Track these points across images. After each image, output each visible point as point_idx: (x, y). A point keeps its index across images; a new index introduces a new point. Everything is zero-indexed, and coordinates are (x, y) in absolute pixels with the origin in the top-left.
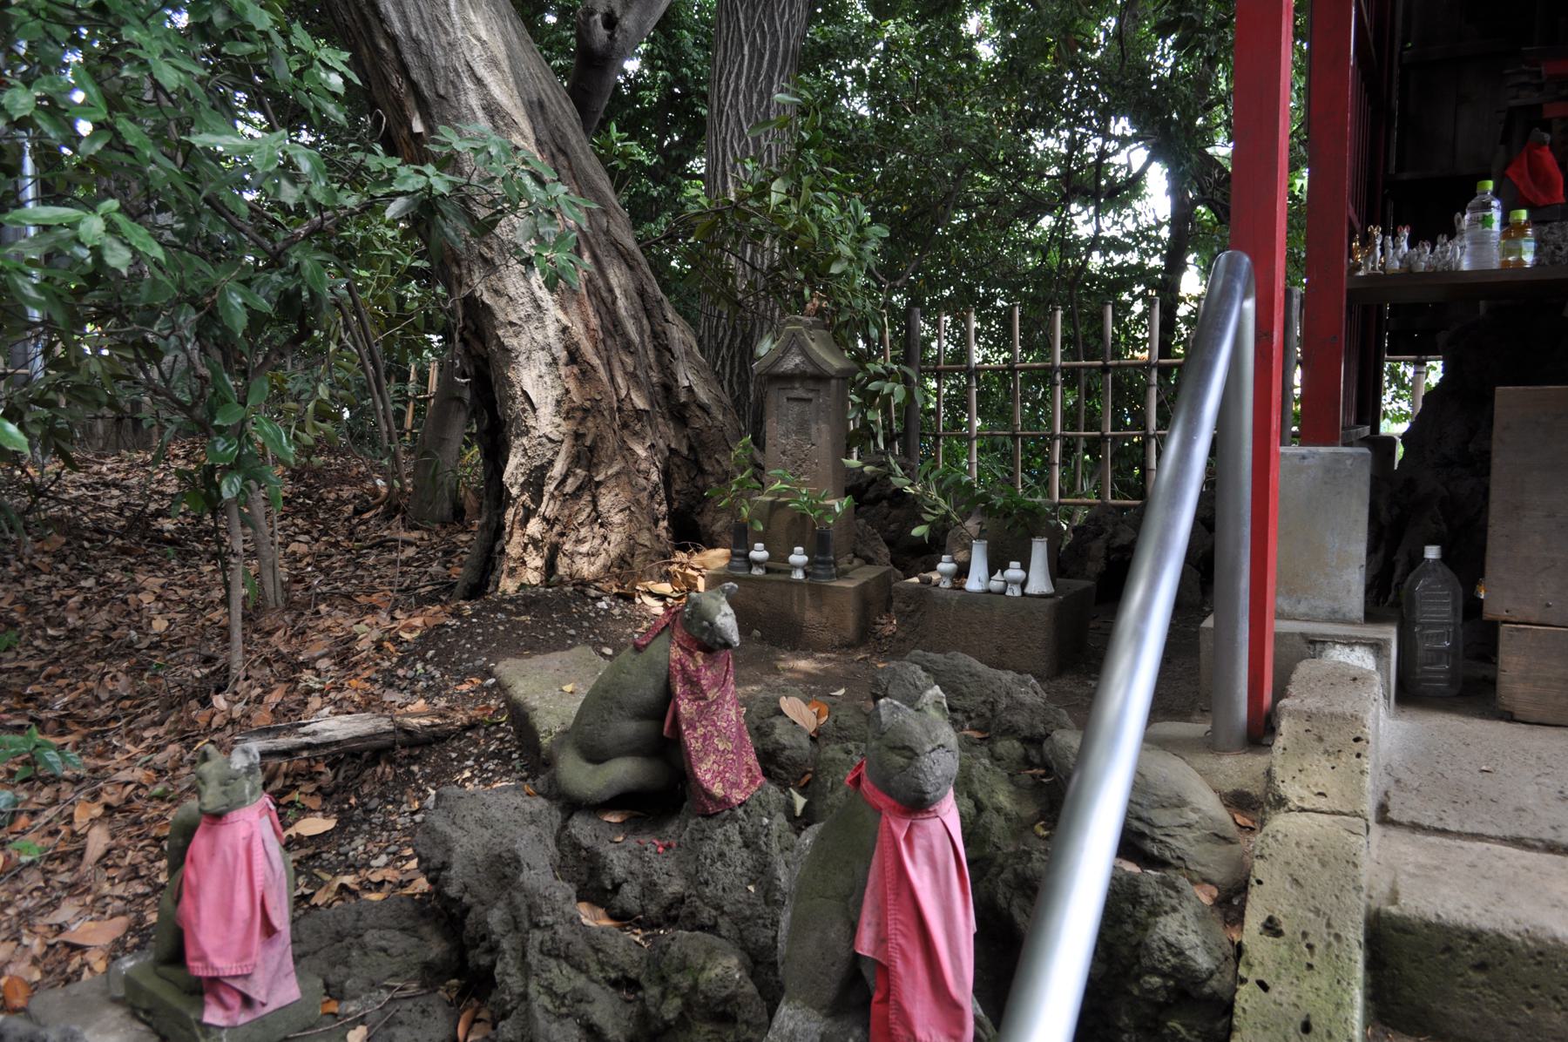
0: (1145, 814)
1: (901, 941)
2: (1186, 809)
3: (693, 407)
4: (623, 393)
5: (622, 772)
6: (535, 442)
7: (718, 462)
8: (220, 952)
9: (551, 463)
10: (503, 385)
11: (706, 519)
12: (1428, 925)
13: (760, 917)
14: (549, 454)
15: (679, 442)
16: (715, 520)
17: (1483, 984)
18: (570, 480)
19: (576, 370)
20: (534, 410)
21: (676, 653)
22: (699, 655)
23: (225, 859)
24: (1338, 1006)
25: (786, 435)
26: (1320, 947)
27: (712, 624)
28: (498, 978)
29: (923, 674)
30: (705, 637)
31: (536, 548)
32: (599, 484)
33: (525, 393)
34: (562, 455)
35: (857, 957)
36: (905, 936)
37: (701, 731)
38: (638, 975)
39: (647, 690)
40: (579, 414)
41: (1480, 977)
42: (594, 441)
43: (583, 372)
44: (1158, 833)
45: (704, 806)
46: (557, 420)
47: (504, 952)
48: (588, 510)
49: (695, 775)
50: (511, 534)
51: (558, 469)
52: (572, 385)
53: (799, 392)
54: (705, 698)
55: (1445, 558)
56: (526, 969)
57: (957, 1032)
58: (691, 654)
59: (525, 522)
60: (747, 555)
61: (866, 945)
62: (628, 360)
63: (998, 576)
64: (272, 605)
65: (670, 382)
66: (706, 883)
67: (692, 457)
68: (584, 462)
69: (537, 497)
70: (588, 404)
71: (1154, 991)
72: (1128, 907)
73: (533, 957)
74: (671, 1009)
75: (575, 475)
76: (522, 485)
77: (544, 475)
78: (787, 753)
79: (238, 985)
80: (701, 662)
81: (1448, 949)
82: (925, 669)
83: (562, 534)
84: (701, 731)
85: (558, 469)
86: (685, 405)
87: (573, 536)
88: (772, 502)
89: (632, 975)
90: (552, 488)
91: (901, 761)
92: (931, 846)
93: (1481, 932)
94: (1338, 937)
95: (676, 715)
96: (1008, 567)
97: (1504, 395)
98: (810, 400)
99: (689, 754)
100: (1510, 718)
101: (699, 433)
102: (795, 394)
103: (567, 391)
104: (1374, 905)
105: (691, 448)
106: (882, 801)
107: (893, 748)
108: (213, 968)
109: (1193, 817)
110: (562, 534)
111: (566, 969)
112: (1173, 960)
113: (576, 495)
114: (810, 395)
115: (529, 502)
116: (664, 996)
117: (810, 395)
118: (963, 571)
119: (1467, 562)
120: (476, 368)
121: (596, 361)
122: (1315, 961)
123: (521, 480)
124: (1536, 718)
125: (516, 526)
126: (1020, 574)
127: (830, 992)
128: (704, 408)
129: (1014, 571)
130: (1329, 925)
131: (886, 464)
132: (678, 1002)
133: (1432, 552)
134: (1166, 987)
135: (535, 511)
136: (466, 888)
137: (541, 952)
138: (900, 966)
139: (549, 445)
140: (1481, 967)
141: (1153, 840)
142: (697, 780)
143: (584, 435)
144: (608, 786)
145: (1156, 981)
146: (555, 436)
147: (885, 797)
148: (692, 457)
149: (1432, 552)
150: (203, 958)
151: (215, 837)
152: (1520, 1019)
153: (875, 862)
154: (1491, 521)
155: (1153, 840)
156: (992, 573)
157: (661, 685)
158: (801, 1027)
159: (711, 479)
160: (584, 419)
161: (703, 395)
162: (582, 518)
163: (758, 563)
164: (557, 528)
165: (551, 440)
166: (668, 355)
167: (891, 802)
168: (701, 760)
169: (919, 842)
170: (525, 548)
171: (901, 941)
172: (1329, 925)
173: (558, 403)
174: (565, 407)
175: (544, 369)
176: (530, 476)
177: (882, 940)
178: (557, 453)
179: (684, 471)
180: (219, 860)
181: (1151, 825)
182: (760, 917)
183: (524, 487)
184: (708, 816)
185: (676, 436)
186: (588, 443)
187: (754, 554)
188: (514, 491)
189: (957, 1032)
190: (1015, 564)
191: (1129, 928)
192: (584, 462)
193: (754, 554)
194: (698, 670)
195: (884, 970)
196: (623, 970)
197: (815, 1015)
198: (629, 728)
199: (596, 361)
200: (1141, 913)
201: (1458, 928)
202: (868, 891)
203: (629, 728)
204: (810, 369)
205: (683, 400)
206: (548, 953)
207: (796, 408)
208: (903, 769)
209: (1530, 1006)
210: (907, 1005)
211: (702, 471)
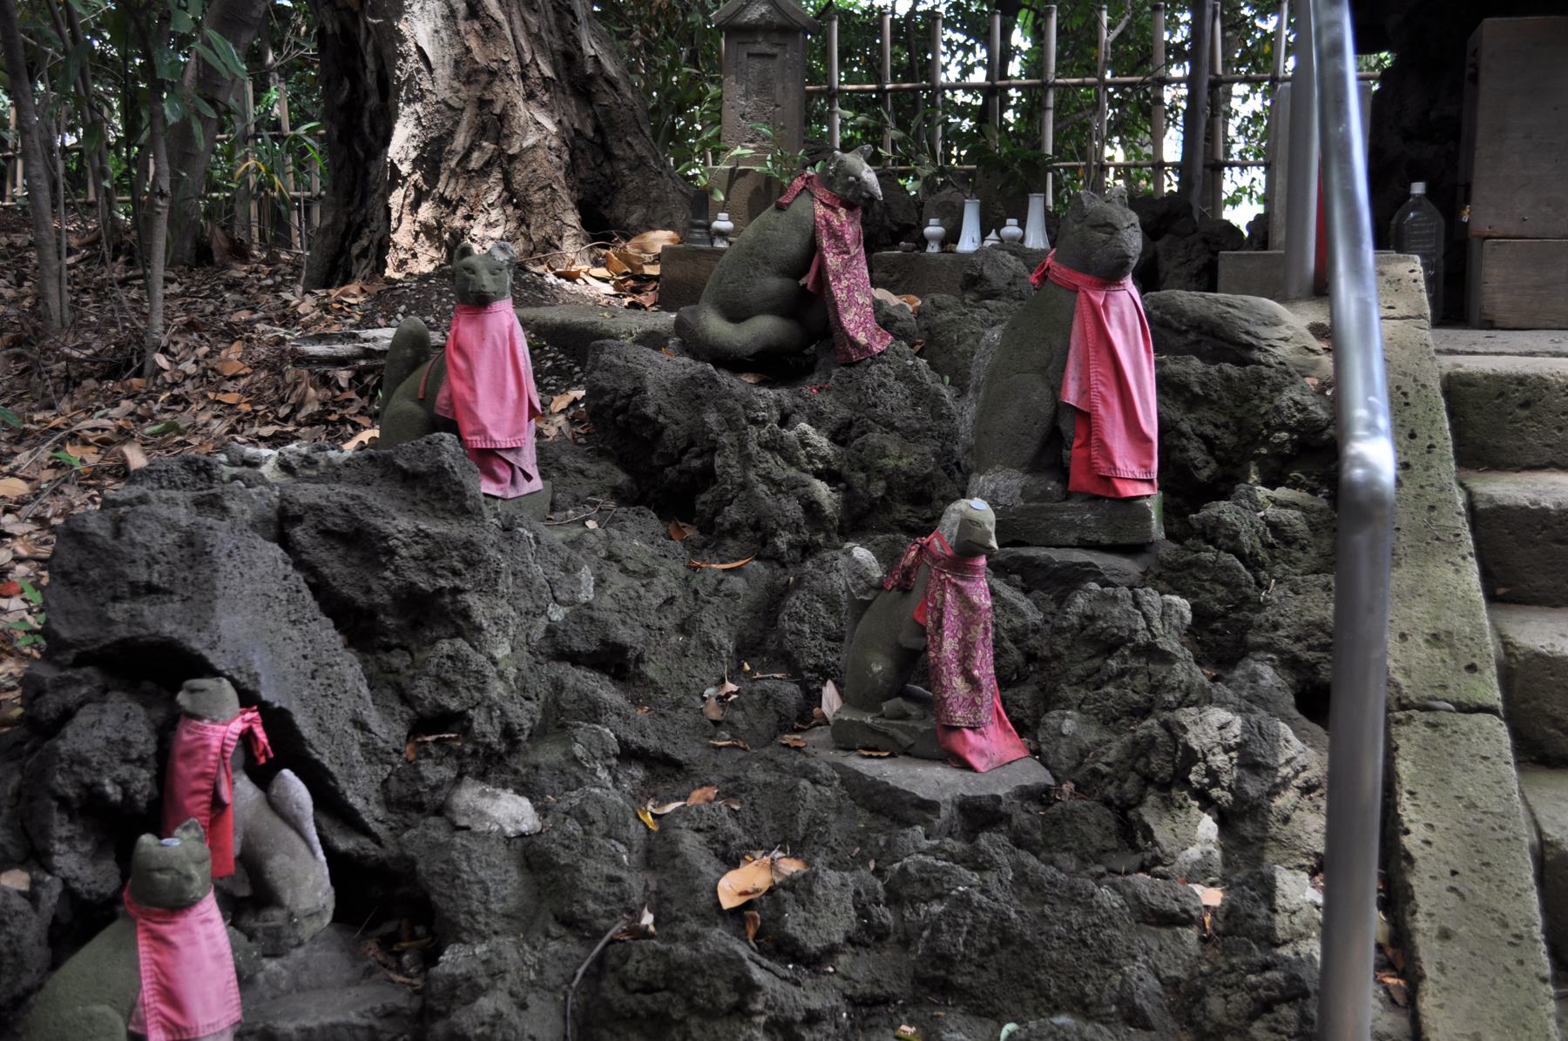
0: (1252, 329)
1: (1102, 389)
2: (1282, 327)
3: (600, 81)
4: (528, 58)
5: (763, 328)
6: (431, 109)
7: (630, 145)
8: (496, 426)
9: (451, 134)
10: (392, 40)
11: (620, 211)
12: (1487, 377)
13: (929, 429)
14: (449, 124)
15: (582, 122)
16: (628, 213)
17: (1527, 418)
18: (476, 155)
19: (477, 26)
20: (431, 70)
21: (820, 210)
22: (842, 211)
23: (495, 344)
24: (1433, 422)
25: (746, 95)
26: (1412, 393)
27: (858, 179)
28: (718, 471)
29: (1012, 258)
30: (849, 194)
31: (429, 236)
32: (512, 158)
33: (420, 50)
34: (464, 124)
35: (1060, 408)
36: (1104, 385)
37: (845, 283)
38: (841, 467)
39: (793, 245)
40: (484, 78)
41: (1526, 413)
42: (504, 109)
43: (487, 29)
44: (1263, 344)
45: (848, 354)
46: (456, 84)
47: (724, 447)
48: (499, 189)
49: (840, 323)
50: (400, 220)
51: (460, 141)
52: (473, 43)
53: (762, 47)
54: (848, 252)
55: (1430, 193)
56: (747, 460)
57: (1146, 462)
58: (834, 210)
59: (415, 206)
60: (708, 227)
61: (1071, 395)
62: (532, 19)
63: (993, 235)
64: (57, 325)
65: (573, 49)
66: (875, 406)
67: (598, 140)
68: (491, 134)
69: (432, 176)
70: (494, 65)
71: (1282, 444)
72: (1253, 388)
73: (753, 448)
74: (878, 489)
75: (481, 148)
76: (414, 161)
77: (441, 150)
78: (898, 324)
79: (510, 458)
80: (844, 218)
81: (1501, 394)
82: (1011, 253)
83: (468, 218)
84: (845, 283)
85: (460, 141)
86: (591, 78)
87: (482, 219)
88: (732, 170)
89: (835, 467)
90: (453, 164)
91: (1104, 236)
92: (1122, 313)
93: (1527, 377)
94: (1424, 386)
95: (822, 267)
96: (1004, 225)
97: (1494, 33)
98: (773, 56)
99: (836, 304)
100: (1489, 325)
101: (607, 111)
102: (757, 49)
103: (468, 50)
104: (1445, 372)
105: (598, 129)
106: (1079, 279)
107: (1094, 227)
108: (492, 440)
109: (1289, 333)
110: (468, 218)
111: (780, 461)
112: (1299, 416)
113: (483, 172)
114: (775, 50)
115: (421, 182)
116: (869, 480)
117: (775, 50)
118: (953, 236)
119: (1451, 195)
120: (342, 24)
121: (500, 17)
122: (1410, 400)
123: (413, 155)
124: (1513, 324)
125: (406, 210)
126: (1017, 231)
127: (1030, 450)
128: (611, 82)
129: (1011, 229)
130: (1415, 380)
131: (878, 115)
132: (882, 484)
133: (1418, 188)
134: (1291, 440)
135: (428, 192)
136: (660, 410)
137: (759, 444)
138: (1101, 410)
139: (449, 113)
140: (1526, 405)
141: (1260, 349)
142: (843, 328)
143: (491, 102)
144: (755, 340)
145: (1285, 435)
146: (455, 103)
147: (1081, 276)
148: (598, 140)
149: (1418, 188)
150: (482, 431)
151: (482, 324)
152: (1553, 441)
153: (1076, 327)
154: (1478, 144)
155: (1260, 349)
156: (984, 234)
157: (807, 239)
158: (1002, 485)
159: (623, 165)
160: (490, 83)
161: (611, 68)
162: (492, 197)
163: (722, 234)
164: (462, 211)
165: (450, 107)
166: (570, 18)
167: (1087, 278)
168: (846, 310)
169: (1113, 309)
170: (416, 238)
171: (1102, 389)
172: (1415, 380)
173: (457, 63)
174: (466, 69)
175: (440, 23)
176: (423, 150)
177: (1085, 391)
178: (457, 123)
179: (589, 156)
180: (488, 344)
181: (1257, 337)
182: (929, 429)
183: (416, 164)
184: (851, 364)
185: (578, 115)
186: (498, 110)
187: (717, 225)
188: (405, 169)
189: (1146, 462)
190: (1012, 221)
191: (1256, 402)
192: (491, 134)
193: (717, 225)
194: (842, 225)
195: (1085, 417)
196: (828, 462)
197: (1015, 473)
198: (773, 284)
199: (500, 17)
200: (1265, 391)
201: (1509, 376)
202: (1071, 352)
203: (773, 284)
204: (777, 19)
205: (589, 71)
206: (765, 446)
207: (757, 65)
208: (1105, 242)
209: (1560, 429)
210: (1108, 440)
211: (610, 157)
